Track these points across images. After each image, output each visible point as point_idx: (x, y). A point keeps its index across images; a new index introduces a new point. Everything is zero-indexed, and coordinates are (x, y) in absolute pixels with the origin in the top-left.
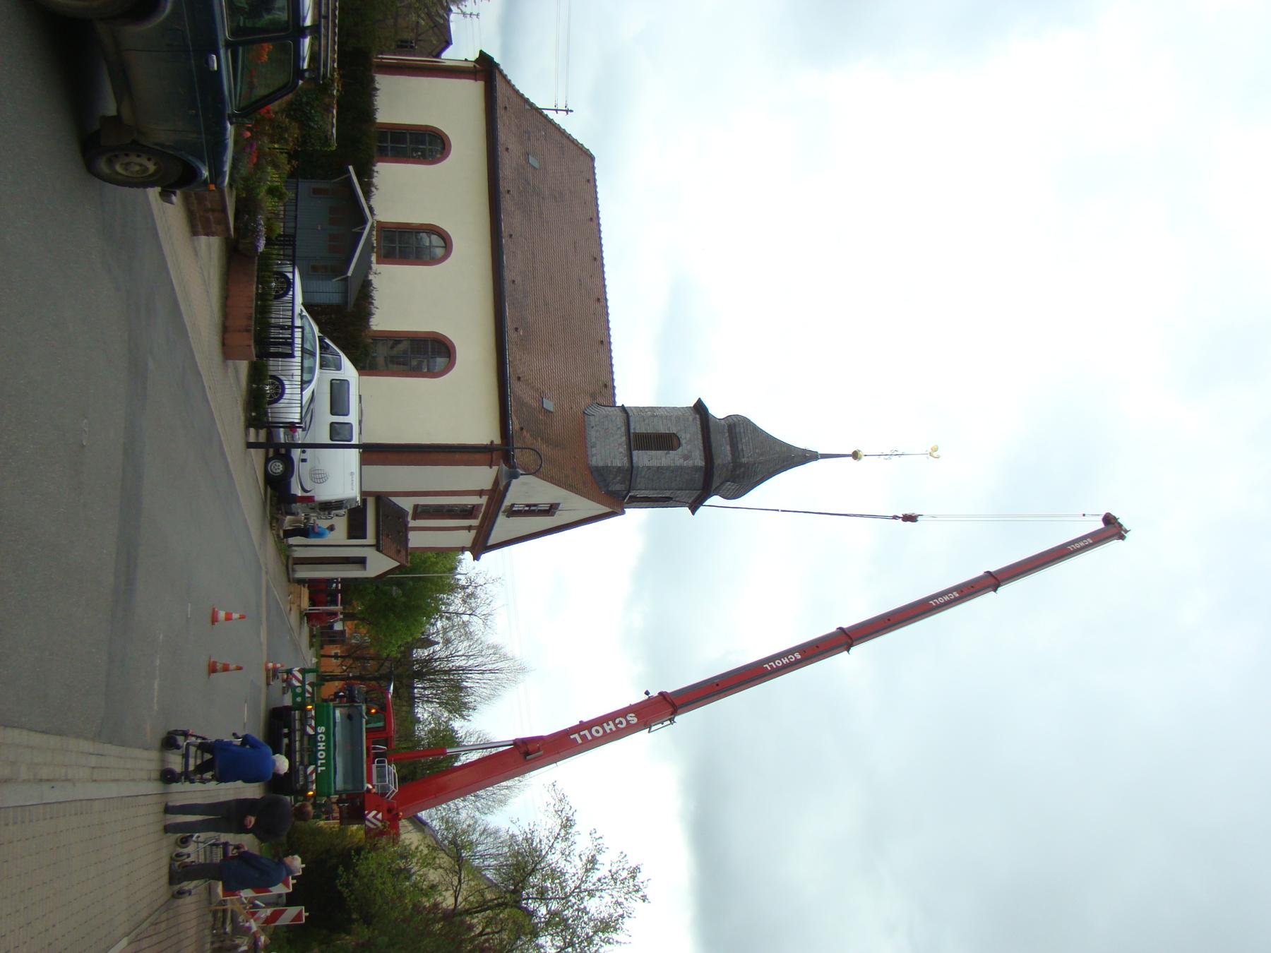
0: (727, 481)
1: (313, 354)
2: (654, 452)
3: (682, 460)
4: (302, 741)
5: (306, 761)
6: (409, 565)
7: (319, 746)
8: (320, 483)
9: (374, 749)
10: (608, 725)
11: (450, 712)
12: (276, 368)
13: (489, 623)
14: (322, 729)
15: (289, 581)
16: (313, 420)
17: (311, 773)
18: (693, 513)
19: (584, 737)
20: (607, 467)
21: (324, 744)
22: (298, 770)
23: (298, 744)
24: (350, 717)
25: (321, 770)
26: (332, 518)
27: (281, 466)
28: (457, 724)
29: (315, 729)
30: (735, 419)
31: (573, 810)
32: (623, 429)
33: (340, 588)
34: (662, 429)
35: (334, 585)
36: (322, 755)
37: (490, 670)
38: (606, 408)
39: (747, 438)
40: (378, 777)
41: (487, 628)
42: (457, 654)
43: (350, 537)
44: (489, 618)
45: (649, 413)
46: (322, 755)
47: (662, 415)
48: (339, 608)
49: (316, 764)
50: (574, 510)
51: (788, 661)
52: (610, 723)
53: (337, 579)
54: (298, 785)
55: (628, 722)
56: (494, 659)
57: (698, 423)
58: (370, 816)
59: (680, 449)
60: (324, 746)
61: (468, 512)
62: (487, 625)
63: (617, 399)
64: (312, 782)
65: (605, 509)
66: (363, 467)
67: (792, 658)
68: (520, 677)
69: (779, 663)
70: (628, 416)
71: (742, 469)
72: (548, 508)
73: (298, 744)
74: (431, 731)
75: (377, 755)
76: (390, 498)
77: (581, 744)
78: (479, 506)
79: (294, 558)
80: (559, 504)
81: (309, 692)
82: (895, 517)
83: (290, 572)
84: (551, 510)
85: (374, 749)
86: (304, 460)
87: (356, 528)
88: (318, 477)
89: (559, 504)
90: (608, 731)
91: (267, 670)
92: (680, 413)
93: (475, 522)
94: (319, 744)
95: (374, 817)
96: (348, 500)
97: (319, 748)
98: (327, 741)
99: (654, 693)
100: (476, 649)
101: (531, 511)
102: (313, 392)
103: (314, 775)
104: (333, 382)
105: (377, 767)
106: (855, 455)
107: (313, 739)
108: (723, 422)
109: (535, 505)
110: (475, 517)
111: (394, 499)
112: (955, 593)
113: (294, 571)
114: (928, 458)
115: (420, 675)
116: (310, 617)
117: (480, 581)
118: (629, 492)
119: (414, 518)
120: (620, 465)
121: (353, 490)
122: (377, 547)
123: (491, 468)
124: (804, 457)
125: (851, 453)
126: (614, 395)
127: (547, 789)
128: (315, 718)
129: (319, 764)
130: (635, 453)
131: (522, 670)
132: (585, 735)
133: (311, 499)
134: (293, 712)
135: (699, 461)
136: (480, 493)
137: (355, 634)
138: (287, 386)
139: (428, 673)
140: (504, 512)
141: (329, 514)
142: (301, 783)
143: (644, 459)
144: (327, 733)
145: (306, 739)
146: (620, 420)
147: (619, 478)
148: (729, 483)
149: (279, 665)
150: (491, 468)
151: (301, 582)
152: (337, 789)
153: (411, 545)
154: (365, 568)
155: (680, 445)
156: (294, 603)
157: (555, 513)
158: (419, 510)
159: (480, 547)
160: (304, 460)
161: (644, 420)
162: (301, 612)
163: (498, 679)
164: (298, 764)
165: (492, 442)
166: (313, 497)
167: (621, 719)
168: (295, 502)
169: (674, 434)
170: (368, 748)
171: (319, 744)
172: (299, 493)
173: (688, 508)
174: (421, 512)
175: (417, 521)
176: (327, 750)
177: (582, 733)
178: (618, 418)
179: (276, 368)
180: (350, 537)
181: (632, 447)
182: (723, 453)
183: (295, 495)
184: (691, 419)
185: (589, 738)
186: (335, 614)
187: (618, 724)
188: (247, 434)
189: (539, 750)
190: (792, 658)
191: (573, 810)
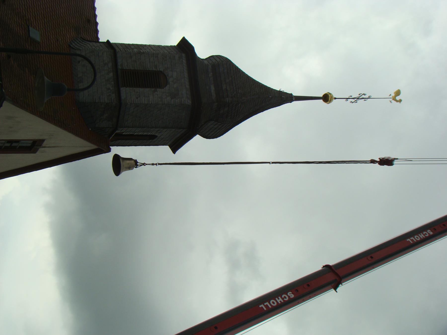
2: (141, 90)
10: (279, 299)
21: (282, 301)
30: (218, 60)
32: (110, 65)
38: (91, 44)
45: (135, 50)
50: (58, 147)
51: (282, 301)
57: (184, 61)
59: (167, 88)
63: (100, 36)
72: (30, 145)
80: (43, 141)
82: (373, 161)
89: (43, 141)
92: (166, 52)
94: (279, 298)
97: (277, 299)
106: (326, 98)
108: (206, 62)
109: (17, 141)
112: (429, 231)
125: (321, 96)
126: (97, 32)
130: (123, 90)
132: (267, 305)
155: (167, 83)
157: (38, 149)
169: (161, 71)
173: (167, 147)
190: (286, 298)
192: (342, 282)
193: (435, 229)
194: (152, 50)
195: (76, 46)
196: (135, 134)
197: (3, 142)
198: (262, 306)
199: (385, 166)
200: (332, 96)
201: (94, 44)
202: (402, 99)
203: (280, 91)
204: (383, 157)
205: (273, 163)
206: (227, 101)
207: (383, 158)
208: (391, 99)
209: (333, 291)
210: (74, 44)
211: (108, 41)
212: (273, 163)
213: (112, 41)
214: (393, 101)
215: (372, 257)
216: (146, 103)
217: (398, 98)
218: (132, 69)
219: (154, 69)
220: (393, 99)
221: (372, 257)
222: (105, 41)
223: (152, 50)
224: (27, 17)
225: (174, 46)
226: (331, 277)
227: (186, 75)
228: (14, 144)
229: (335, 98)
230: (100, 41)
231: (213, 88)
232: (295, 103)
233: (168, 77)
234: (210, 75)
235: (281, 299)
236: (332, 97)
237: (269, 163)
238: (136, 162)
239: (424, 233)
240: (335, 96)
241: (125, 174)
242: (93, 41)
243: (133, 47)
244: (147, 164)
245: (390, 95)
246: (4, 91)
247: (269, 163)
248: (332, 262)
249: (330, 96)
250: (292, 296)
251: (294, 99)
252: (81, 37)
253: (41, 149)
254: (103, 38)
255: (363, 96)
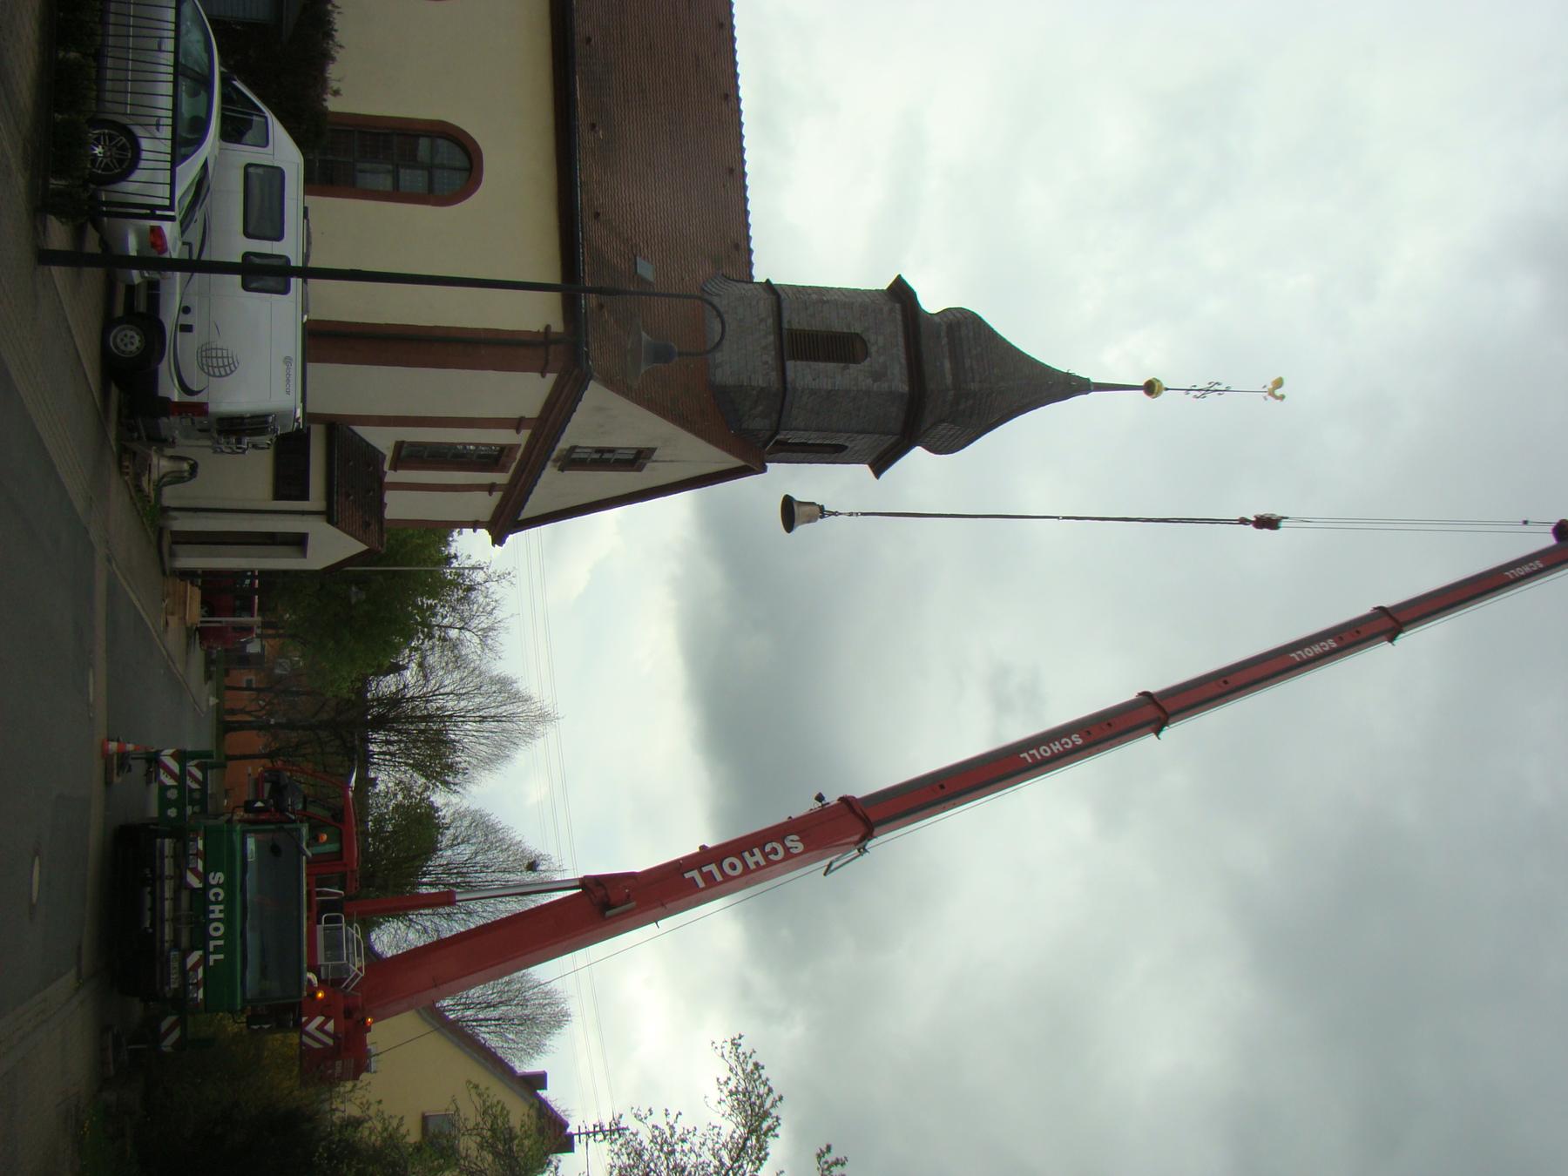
0: (943, 421)
1: (205, 83)
2: (821, 365)
3: (869, 381)
4: (176, 899)
5: (185, 941)
6: (383, 551)
7: (213, 912)
8: (221, 376)
9: (318, 894)
10: (752, 855)
11: (427, 777)
12: (120, 108)
13: (489, 642)
14: (218, 877)
15: (164, 573)
16: (207, 243)
17: (195, 967)
18: (878, 473)
19: (709, 878)
20: (741, 386)
21: (221, 907)
22: (168, 960)
23: (168, 905)
24: (275, 850)
25: (215, 961)
26: (245, 450)
27: (137, 338)
28: (439, 798)
29: (204, 878)
30: (958, 315)
31: (775, 1095)
32: (770, 321)
33: (257, 586)
34: (838, 326)
35: (248, 582)
36: (217, 929)
37: (492, 717)
38: (739, 285)
39: (979, 349)
40: (327, 948)
41: (487, 651)
42: (442, 691)
43: (278, 495)
44: (490, 634)
46: (217, 929)
47: (835, 300)
48: (257, 619)
49: (205, 948)
51: (1061, 749)
52: (756, 851)
53: (253, 572)
54: (167, 988)
55: (787, 849)
56: (500, 699)
57: (899, 317)
58: (312, 1027)
59: (867, 363)
60: (221, 911)
61: (491, 459)
62: (487, 645)
63: (754, 272)
64: (197, 985)
65: (734, 462)
66: (310, 366)
67: (1067, 743)
68: (540, 728)
69: (1045, 751)
70: (778, 296)
71: (971, 402)
72: (631, 457)
73: (168, 905)
74: (398, 807)
75: (326, 906)
76: (352, 427)
77: (703, 889)
78: (512, 448)
79: (172, 533)
80: (653, 450)
81: (195, 779)
82: (1243, 521)
83: (166, 556)
84: (637, 459)
85: (318, 894)
86: (187, 328)
87: (290, 483)
88: (217, 363)
89: (653, 450)
90: (752, 866)
91: (106, 756)
92: (867, 300)
93: (501, 478)
94: (212, 907)
95: (321, 1028)
96: (279, 416)
97: (212, 916)
98: (229, 903)
99: (832, 798)
100: (472, 685)
101: (604, 460)
102: (205, 165)
103: (200, 971)
104: (251, 170)
105: (325, 929)
106: (1151, 388)
107: (200, 898)
108: (937, 319)
109: (611, 450)
110: (503, 469)
111: (360, 430)
113: (173, 555)
114: (1265, 398)
115: (380, 723)
116: (204, 634)
117: (479, 576)
118: (777, 433)
119: (394, 467)
120: (764, 385)
121: (288, 393)
122: (330, 515)
123: (543, 376)
124: (1069, 386)
125: (1142, 384)
126: (750, 265)
127: (719, 1050)
128: (205, 855)
129: (211, 949)
130: (790, 364)
131: (543, 717)
132: (710, 872)
133: (201, 409)
134: (159, 840)
135: (899, 382)
136: (518, 424)
137: (281, 661)
138: (144, 155)
139: (397, 719)
140: (555, 461)
141: (239, 442)
142: (174, 986)
143: (803, 374)
144: (228, 886)
145: (185, 896)
146: (765, 305)
147: (761, 408)
148: (946, 424)
149: (130, 747)
150: (543, 376)
151: (188, 575)
152: (249, 996)
153: (389, 514)
154: (304, 554)
155: (866, 354)
156: (172, 614)
157: (645, 465)
158: (404, 453)
159: (502, 526)
160: (187, 328)
161: (807, 309)
162: (188, 629)
163: (504, 730)
164: (167, 945)
165: (548, 328)
166: (206, 404)
167: (775, 844)
168: (167, 415)
169: (858, 334)
170: (309, 893)
171: (212, 907)
172: (176, 396)
173: (867, 466)
174: (409, 456)
175: (399, 472)
176: (228, 921)
177: (705, 869)
178: (762, 303)
179: (120, 108)
180: (278, 495)
181: (785, 354)
182: (942, 370)
183: (167, 400)
184: (886, 309)
185: (719, 877)
186: (248, 630)
187: (770, 853)
188: (38, 230)
189: (628, 899)
190: (1067, 743)
191: (775, 1095)
192: (1170, 721)
193: (1341, 638)
194: (843, 297)
195: (714, 290)
196: (810, 442)
197: (589, 450)
198: (1025, 755)
199: (1266, 531)
200: (1162, 384)
201: (745, 286)
202: (1285, 394)
203: (1068, 374)
204: (1262, 514)
205: (1064, 518)
206: (972, 388)
207: (1262, 516)
208: (1266, 394)
209: (1153, 737)
210: (709, 286)
211: (768, 281)
212: (1064, 518)
213: (774, 282)
214: (1270, 398)
215: (1225, 682)
216: (830, 388)
217: (1278, 392)
218: (807, 329)
219: (845, 330)
220: (1270, 394)
221: (1225, 682)
222: (764, 281)
223: (843, 297)
224: (626, 235)
225: (882, 290)
226: (1150, 712)
227: (901, 340)
228: (606, 456)
229: (1167, 389)
230: (755, 281)
231: (947, 365)
232: (1094, 396)
233: (869, 345)
234: (943, 342)
235: (1058, 746)
236: (1161, 386)
237: (1057, 518)
238: (822, 508)
239: (1322, 644)
240: (1165, 386)
241: (801, 530)
242: (743, 281)
243: (809, 291)
244: (840, 514)
245: (1265, 387)
246: (590, 363)
247: (1057, 518)
248: (1154, 688)
249: (1157, 384)
250: (1079, 742)
251: (1092, 388)
252: (723, 274)
253: (649, 465)
254: (759, 275)
255: (1216, 387)
